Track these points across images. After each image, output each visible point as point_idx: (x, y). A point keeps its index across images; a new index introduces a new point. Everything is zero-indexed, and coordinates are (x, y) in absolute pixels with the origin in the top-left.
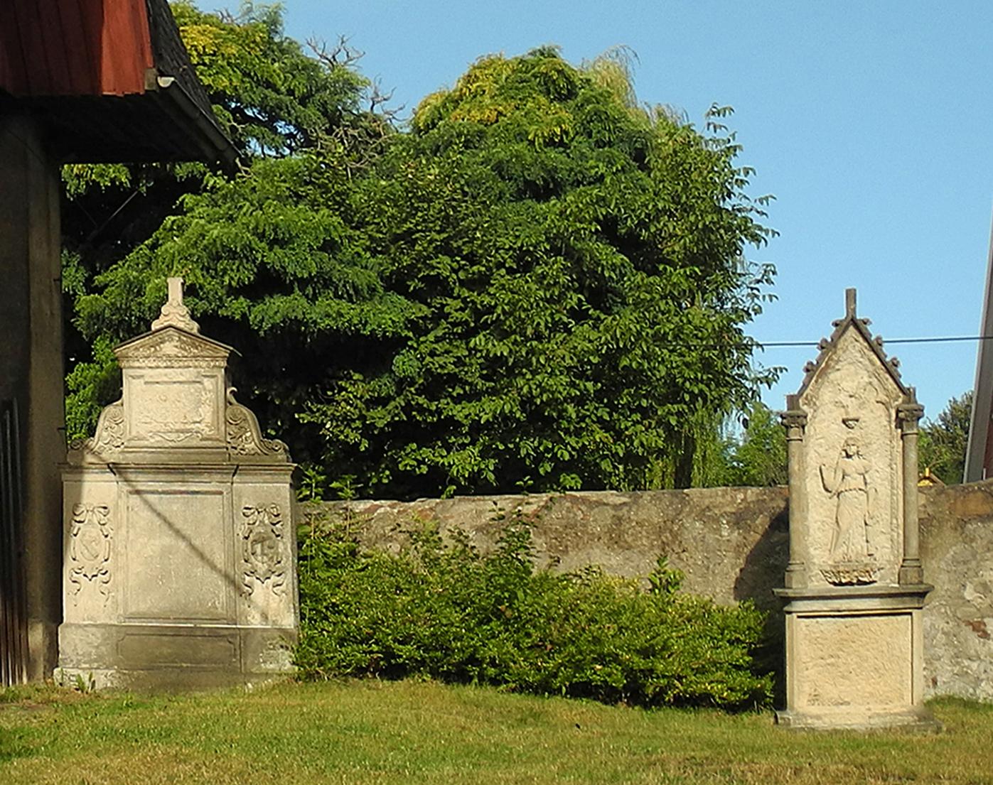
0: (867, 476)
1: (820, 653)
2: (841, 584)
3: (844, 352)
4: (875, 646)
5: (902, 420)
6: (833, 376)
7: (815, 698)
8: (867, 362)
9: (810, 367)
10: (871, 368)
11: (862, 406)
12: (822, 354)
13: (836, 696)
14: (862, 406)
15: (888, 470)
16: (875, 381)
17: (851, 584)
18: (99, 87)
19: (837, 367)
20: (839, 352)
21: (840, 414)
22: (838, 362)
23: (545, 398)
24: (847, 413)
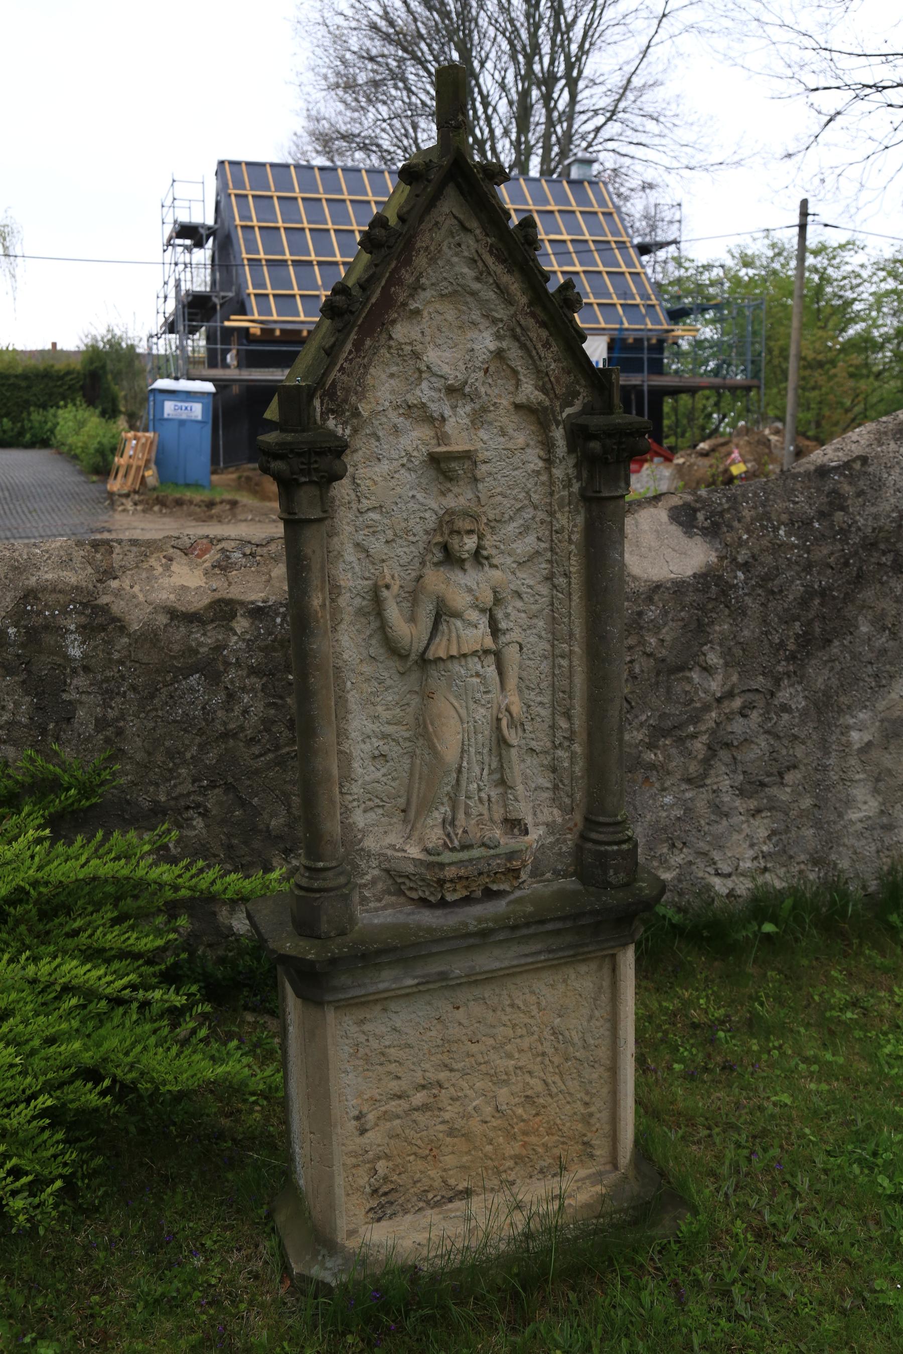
0: (500, 615)
1: (394, 1086)
2: (443, 903)
3: (433, 260)
4: (525, 1043)
5: (850, 469)
6: (401, 331)
7: (385, 1202)
8: (490, 295)
9: (379, 232)
10: (501, 313)
11: (478, 418)
12: (374, 264)
13: (437, 1183)
14: (478, 418)
15: (544, 590)
16: (514, 354)
17: (467, 900)
18: (209, 394)
19: (413, 305)
20: (421, 261)
21: (416, 439)
22: (417, 287)
23: (773, 438)
24: (442, 438)
